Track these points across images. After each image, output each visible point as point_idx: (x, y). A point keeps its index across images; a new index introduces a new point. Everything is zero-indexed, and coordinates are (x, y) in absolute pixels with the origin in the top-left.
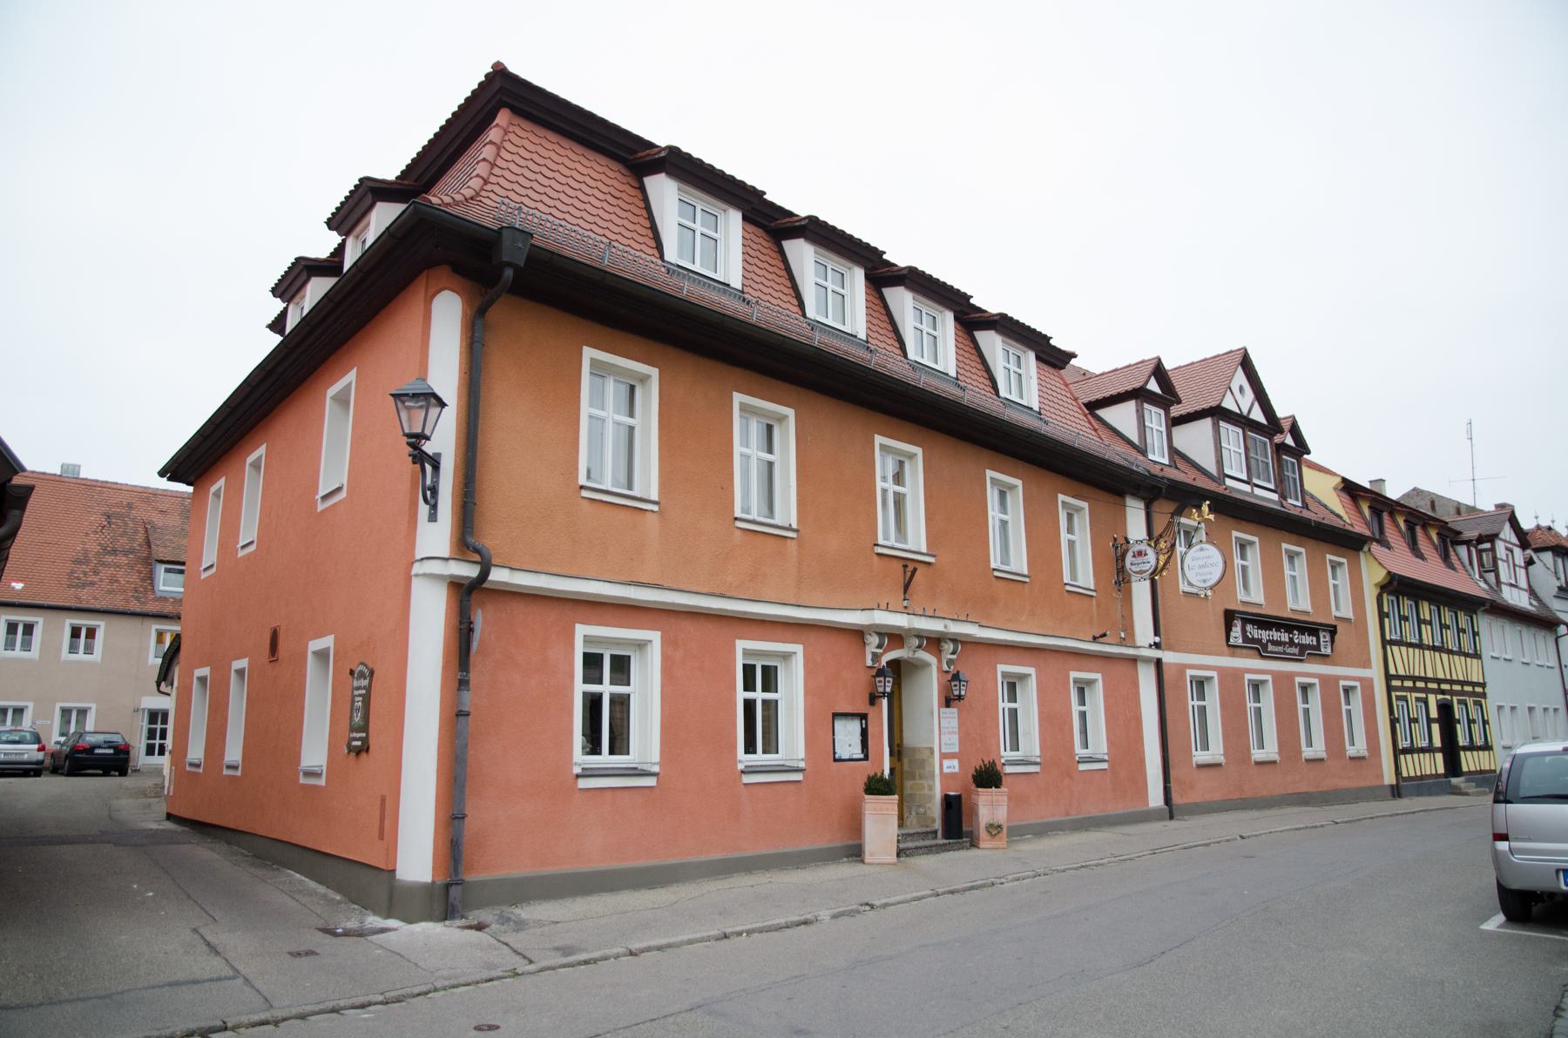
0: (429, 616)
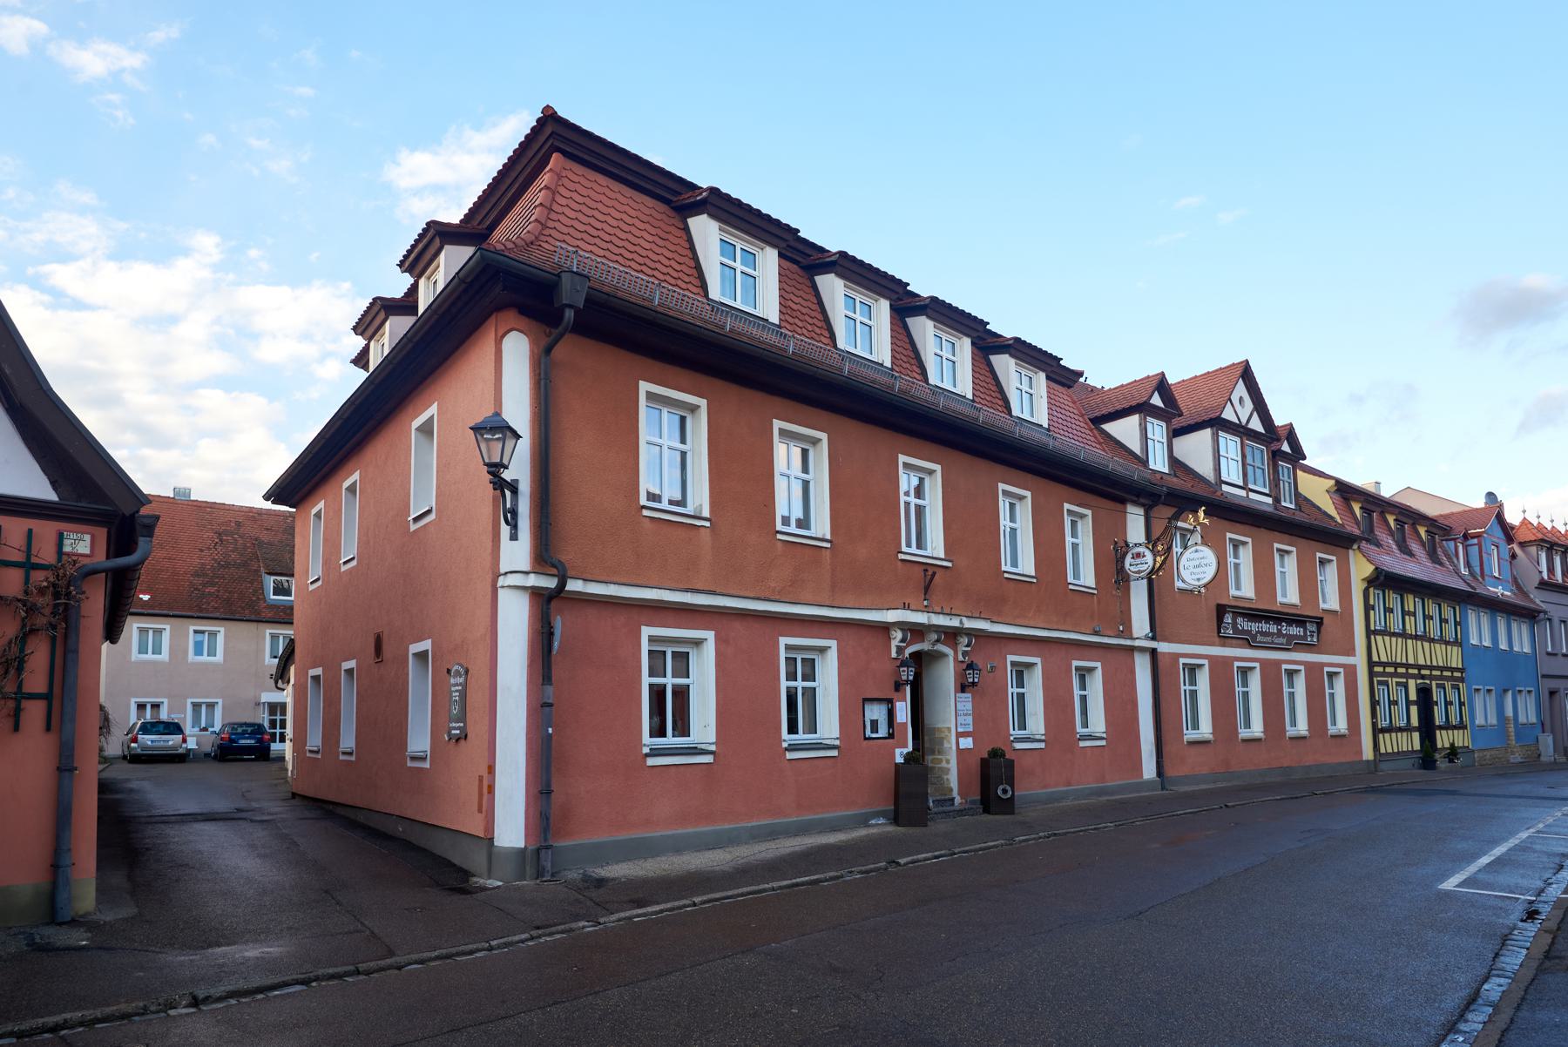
0: (514, 621)
